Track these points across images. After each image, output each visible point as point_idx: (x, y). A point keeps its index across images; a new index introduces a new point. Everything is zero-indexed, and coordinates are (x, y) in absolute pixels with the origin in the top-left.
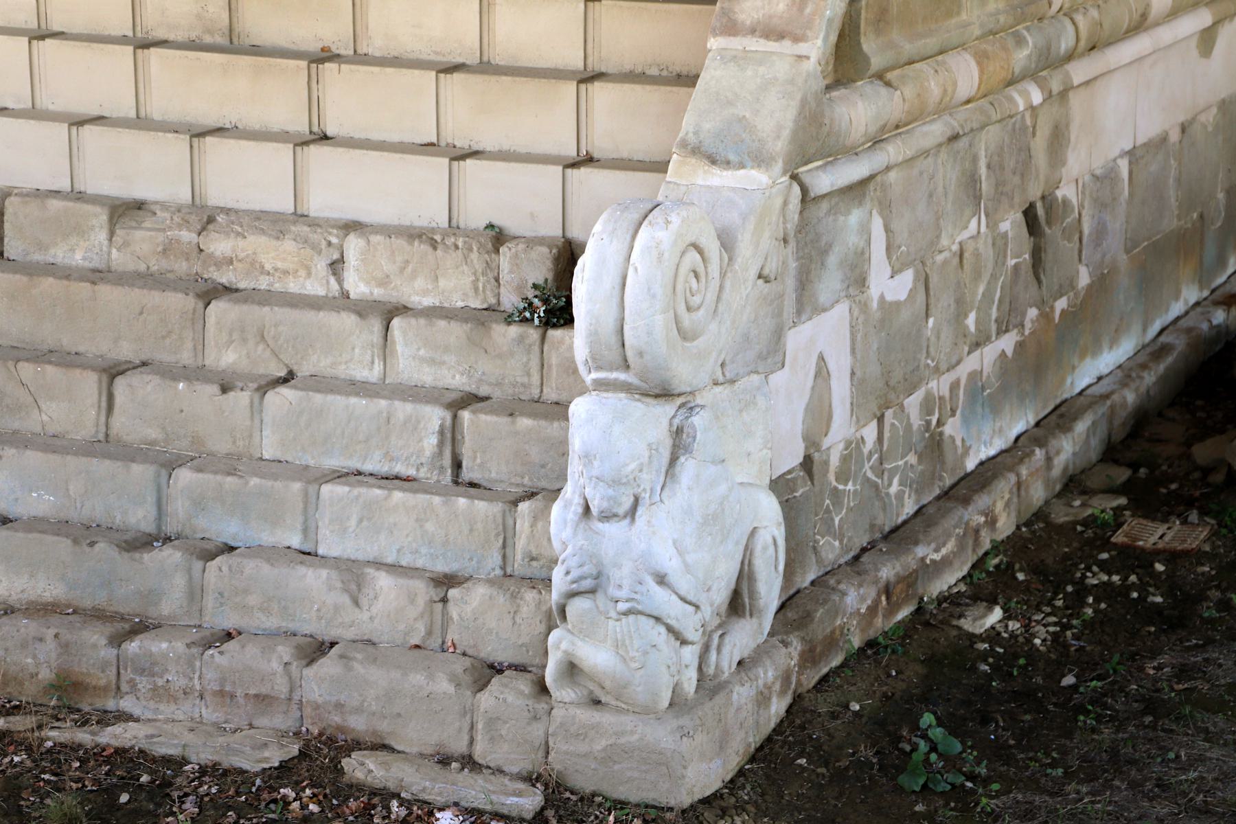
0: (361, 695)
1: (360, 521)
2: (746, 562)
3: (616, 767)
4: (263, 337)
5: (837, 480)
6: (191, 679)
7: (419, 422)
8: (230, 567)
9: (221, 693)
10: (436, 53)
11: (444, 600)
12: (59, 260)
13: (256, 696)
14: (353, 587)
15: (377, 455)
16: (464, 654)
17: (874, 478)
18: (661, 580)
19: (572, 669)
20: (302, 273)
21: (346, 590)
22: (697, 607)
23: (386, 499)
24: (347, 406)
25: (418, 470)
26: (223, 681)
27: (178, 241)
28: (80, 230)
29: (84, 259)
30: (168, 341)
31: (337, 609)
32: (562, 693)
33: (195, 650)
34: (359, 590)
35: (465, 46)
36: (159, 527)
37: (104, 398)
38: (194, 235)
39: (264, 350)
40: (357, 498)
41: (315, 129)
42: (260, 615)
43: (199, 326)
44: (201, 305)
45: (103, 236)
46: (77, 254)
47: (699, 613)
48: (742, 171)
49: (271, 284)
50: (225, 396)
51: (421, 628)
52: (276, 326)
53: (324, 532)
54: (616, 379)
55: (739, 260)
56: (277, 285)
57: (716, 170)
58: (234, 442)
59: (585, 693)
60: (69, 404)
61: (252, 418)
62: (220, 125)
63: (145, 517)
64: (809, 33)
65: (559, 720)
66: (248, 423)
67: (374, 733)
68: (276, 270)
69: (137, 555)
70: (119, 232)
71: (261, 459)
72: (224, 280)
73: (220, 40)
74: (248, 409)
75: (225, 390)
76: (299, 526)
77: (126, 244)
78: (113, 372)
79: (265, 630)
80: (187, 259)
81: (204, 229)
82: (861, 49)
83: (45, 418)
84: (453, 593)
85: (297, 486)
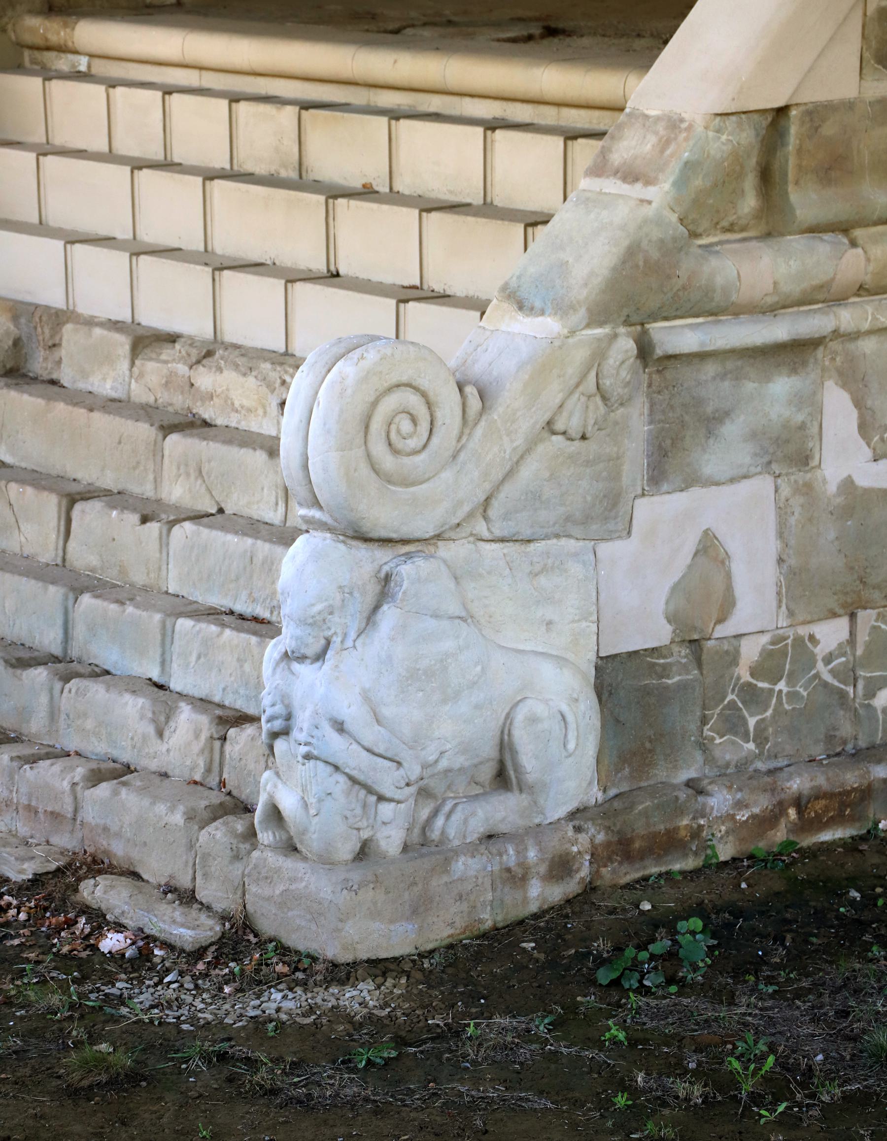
0: (120, 820)
1: (199, 657)
2: (506, 732)
3: (290, 914)
4: (200, 472)
5: (752, 675)
6: (11, 791)
7: (272, 564)
8: (78, 689)
9: (29, 808)
10: (451, 192)
11: (224, 739)
12: (94, 389)
13: (52, 813)
14: (162, 718)
15: (244, 595)
16: (229, 794)
17: (836, 684)
18: (340, 727)
19: (275, 815)
20: (260, 412)
21: (154, 721)
22: (399, 764)
23: (218, 636)
24: (224, 544)
25: (272, 613)
26: (30, 796)
27: (176, 374)
28: (109, 360)
29: (112, 389)
30: (137, 472)
31: (145, 738)
32: (265, 837)
33: (15, 764)
34: (167, 722)
35: (221, 162)
36: (65, 650)
37: (63, 523)
38: (187, 368)
39: (201, 485)
40: (199, 632)
41: (332, 268)
42: (93, 739)
43: (159, 458)
44: (160, 437)
45: (125, 365)
46: (107, 382)
47: (401, 769)
48: (540, 319)
49: (239, 422)
50: (143, 526)
51: (201, 763)
52: (209, 461)
53: (175, 667)
54: (313, 517)
55: (501, 410)
56: (243, 423)
57: (520, 316)
58: (148, 574)
59: (284, 837)
60: (35, 525)
61: (161, 552)
62: (263, 261)
63: (55, 638)
64: (661, 176)
65: (254, 861)
66: (158, 555)
67: (129, 859)
68: (242, 407)
69: (19, 672)
70: (137, 362)
71: (167, 593)
72: (206, 416)
73: (292, 174)
74: (158, 540)
75: (144, 520)
76: (158, 660)
77: (141, 375)
78: (73, 497)
79: (97, 755)
80: (182, 393)
81: (198, 362)
82: (788, 199)
83: (23, 539)
84: (232, 732)
85: (158, 617)
